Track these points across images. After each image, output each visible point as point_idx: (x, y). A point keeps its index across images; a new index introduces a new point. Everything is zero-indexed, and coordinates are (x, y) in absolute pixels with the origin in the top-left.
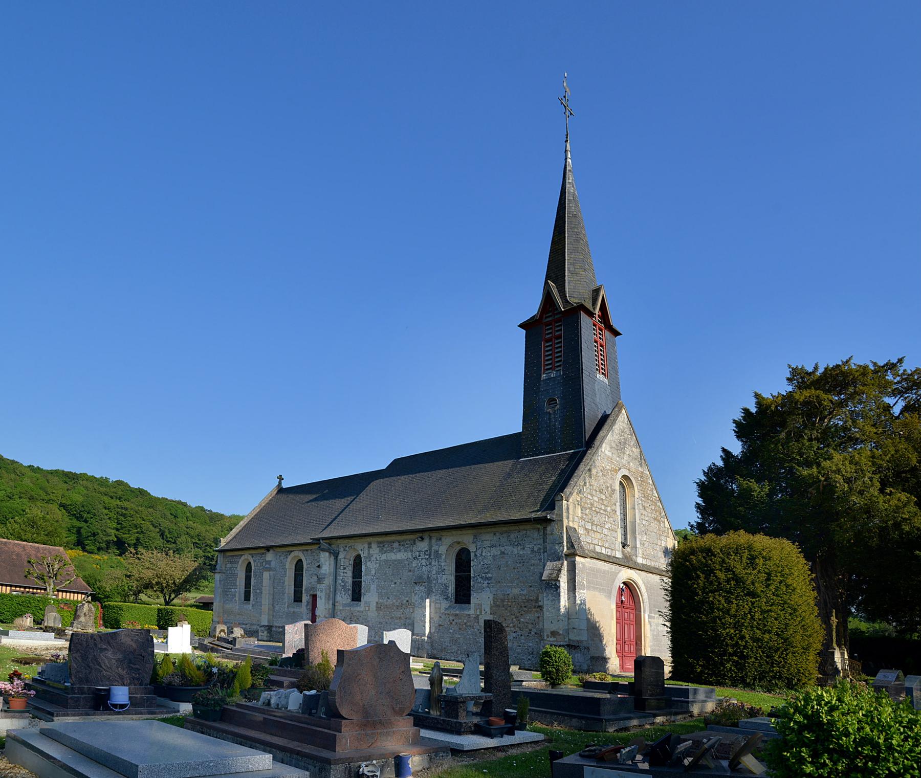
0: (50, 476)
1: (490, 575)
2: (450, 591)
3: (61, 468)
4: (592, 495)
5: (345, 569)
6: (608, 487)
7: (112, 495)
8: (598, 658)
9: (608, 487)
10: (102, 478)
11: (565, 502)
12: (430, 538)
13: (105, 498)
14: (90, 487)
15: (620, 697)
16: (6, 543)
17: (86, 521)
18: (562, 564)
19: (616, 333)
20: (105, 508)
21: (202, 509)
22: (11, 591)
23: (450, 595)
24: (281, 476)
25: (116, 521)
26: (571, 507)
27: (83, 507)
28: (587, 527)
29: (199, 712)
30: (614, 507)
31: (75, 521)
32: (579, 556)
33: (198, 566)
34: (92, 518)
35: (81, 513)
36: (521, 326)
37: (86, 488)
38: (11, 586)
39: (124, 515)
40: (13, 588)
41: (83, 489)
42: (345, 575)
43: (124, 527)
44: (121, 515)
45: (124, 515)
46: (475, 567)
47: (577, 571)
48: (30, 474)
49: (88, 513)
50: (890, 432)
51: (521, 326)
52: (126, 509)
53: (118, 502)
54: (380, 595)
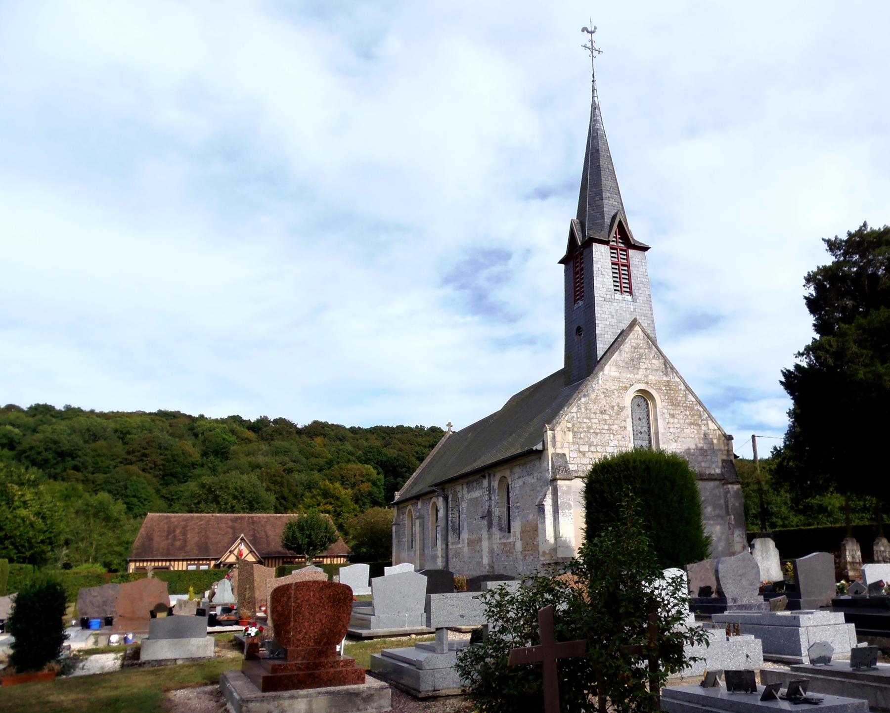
0: (368, 436)
1: (518, 504)
2: (503, 521)
4: (589, 419)
5: (452, 510)
6: (613, 407)
8: (284, 572)
9: (613, 407)
10: (417, 427)
11: (549, 433)
12: (489, 475)
16: (280, 517)
18: (548, 489)
19: (645, 249)
22: (188, 565)
23: (503, 526)
24: (449, 423)
26: (558, 439)
28: (581, 450)
29: (566, 680)
30: (623, 424)
32: (561, 479)
36: (560, 262)
38: (187, 560)
40: (189, 562)
41: (398, 443)
42: (453, 516)
47: (559, 494)
48: (351, 435)
51: (560, 262)
54: (469, 535)
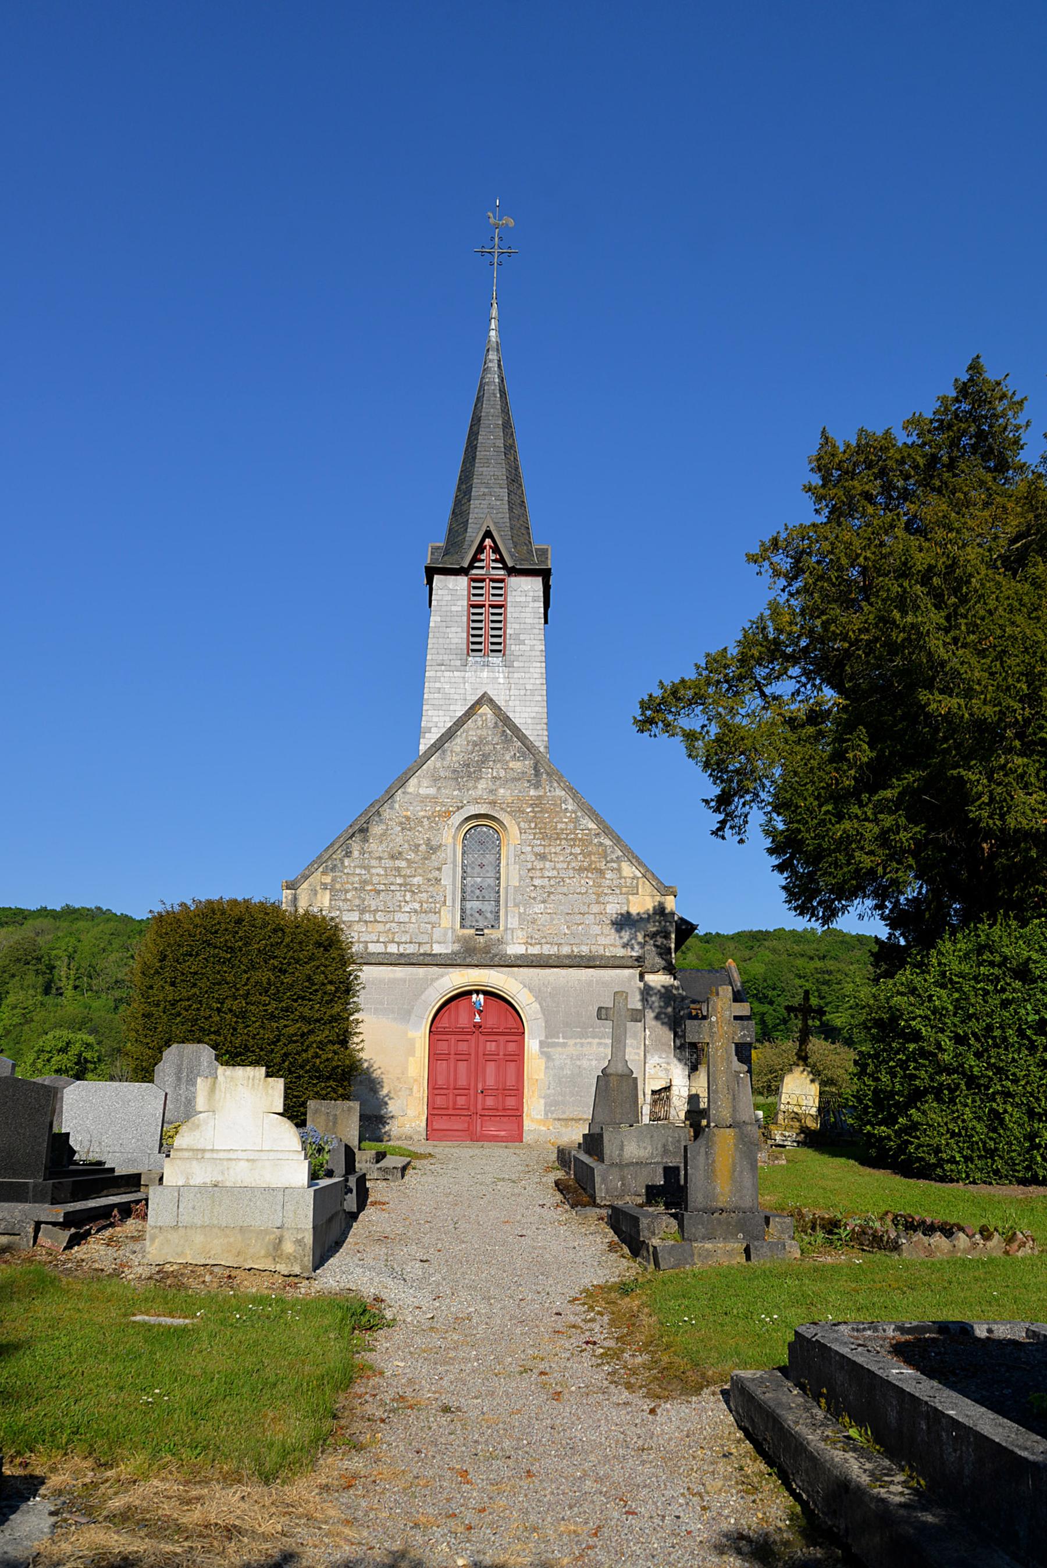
3: (747, 928)
7: (811, 953)
13: (800, 962)
14: (780, 947)
15: (500, 330)
17: (771, 1003)
20: (800, 977)
21: (99, 908)
25: (816, 994)
27: (765, 981)
31: (756, 1004)
33: (546, 1104)
34: (779, 996)
35: (764, 991)
37: (774, 951)
39: (826, 983)
43: (830, 1003)
44: (824, 984)
45: (826, 983)
46: (543, 621)
49: (774, 989)
50: (273, 1510)
52: (830, 973)
53: (819, 964)
